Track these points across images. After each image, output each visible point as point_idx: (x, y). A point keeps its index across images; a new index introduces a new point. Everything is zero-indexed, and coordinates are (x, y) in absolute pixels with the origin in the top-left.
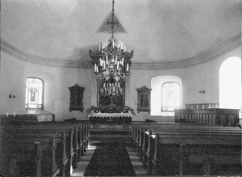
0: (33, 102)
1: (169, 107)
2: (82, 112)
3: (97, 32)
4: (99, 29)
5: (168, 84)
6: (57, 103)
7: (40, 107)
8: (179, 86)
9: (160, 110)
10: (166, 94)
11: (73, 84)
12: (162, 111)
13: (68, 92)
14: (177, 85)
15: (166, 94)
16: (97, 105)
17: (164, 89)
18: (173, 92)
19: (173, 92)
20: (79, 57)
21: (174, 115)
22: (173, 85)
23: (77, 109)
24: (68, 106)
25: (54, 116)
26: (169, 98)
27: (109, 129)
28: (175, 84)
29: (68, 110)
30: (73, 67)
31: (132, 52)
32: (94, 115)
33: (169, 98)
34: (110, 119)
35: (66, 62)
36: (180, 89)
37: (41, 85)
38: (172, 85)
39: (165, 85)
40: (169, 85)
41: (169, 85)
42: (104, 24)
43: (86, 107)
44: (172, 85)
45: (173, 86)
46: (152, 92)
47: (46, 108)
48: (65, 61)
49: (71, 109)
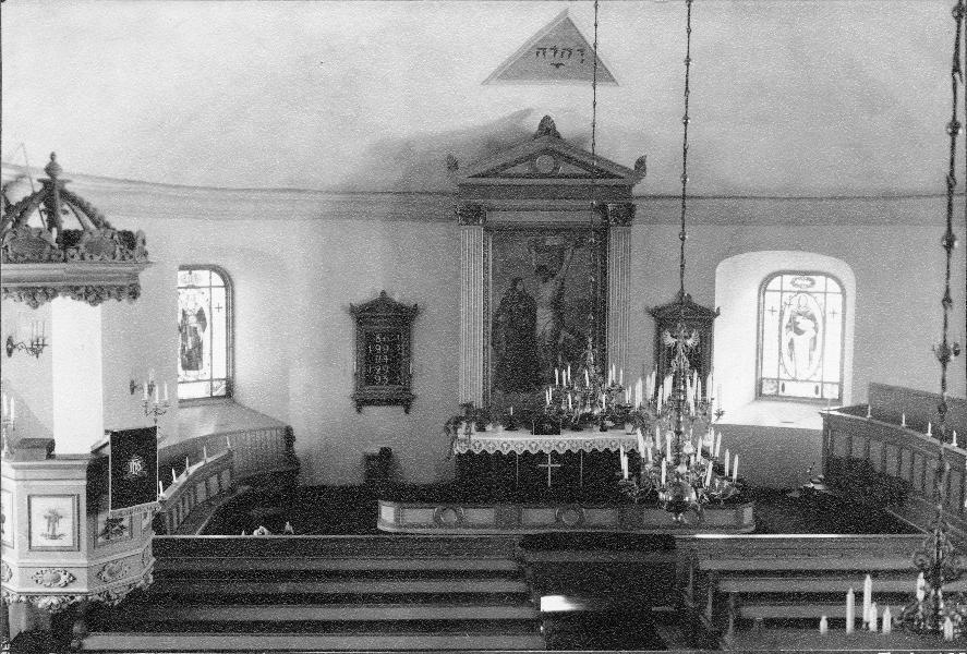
0: (192, 374)
1: (794, 380)
2: (407, 412)
3: (486, 82)
4: (499, 69)
5: (788, 278)
6: (301, 377)
7: (221, 391)
8: (839, 290)
9: (753, 396)
10: (781, 321)
11: (364, 294)
12: (760, 395)
13: (347, 331)
14: (833, 286)
15: (781, 321)
16: (485, 396)
17: (772, 300)
18: (812, 318)
19: (812, 318)
20: (396, 176)
21: (817, 424)
22: (813, 283)
23: (391, 402)
24: (344, 384)
25: (289, 436)
26: (791, 344)
27: (566, 526)
28: (820, 280)
29: (350, 403)
30: (369, 216)
31: (641, 163)
32: (477, 445)
33: (791, 344)
34: (552, 463)
35: (337, 197)
36: (843, 345)
37: (220, 296)
38: (808, 287)
39: (775, 284)
40: (792, 283)
41: (792, 283)
42: (521, 55)
43: (424, 386)
44: (809, 283)
45: (809, 290)
46: (717, 321)
47: (300, 434)
48: (344, 193)
49: (361, 403)
